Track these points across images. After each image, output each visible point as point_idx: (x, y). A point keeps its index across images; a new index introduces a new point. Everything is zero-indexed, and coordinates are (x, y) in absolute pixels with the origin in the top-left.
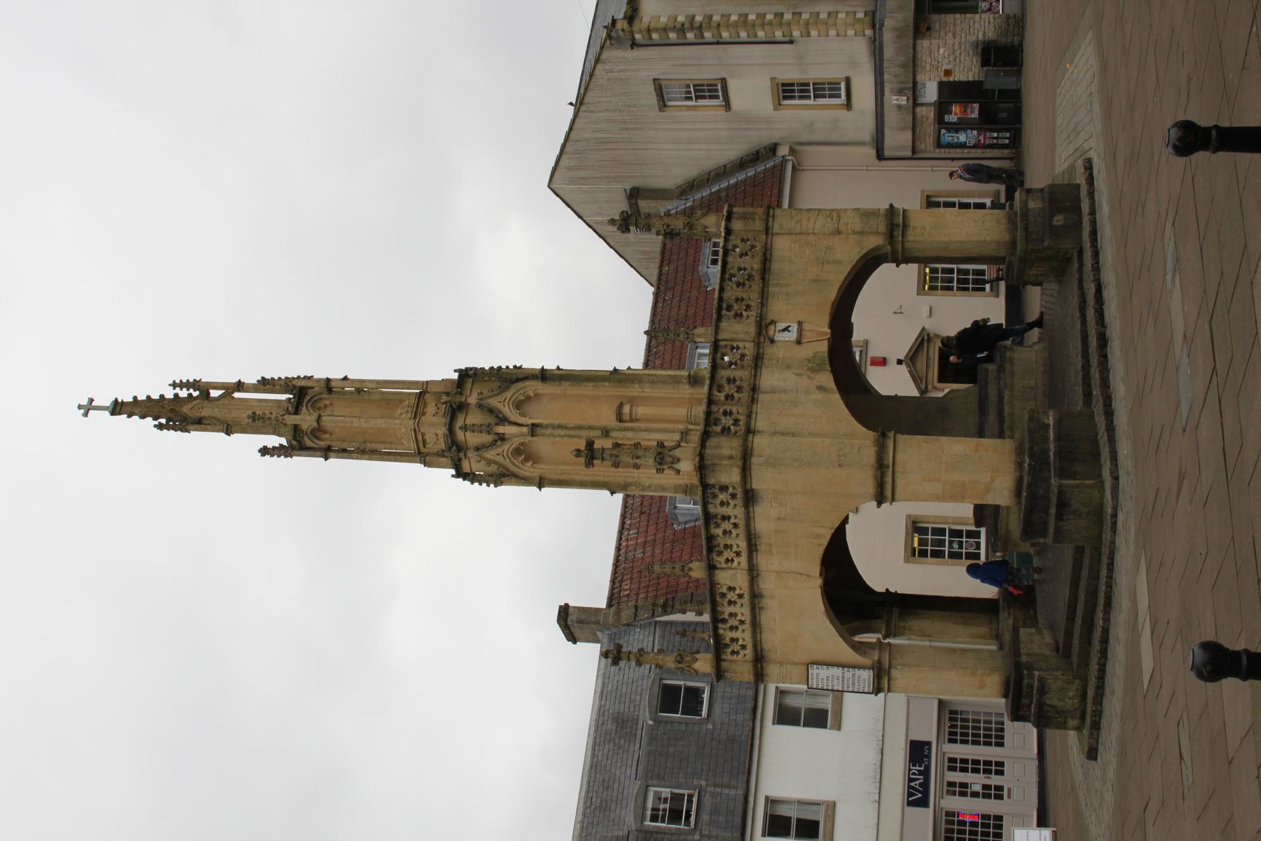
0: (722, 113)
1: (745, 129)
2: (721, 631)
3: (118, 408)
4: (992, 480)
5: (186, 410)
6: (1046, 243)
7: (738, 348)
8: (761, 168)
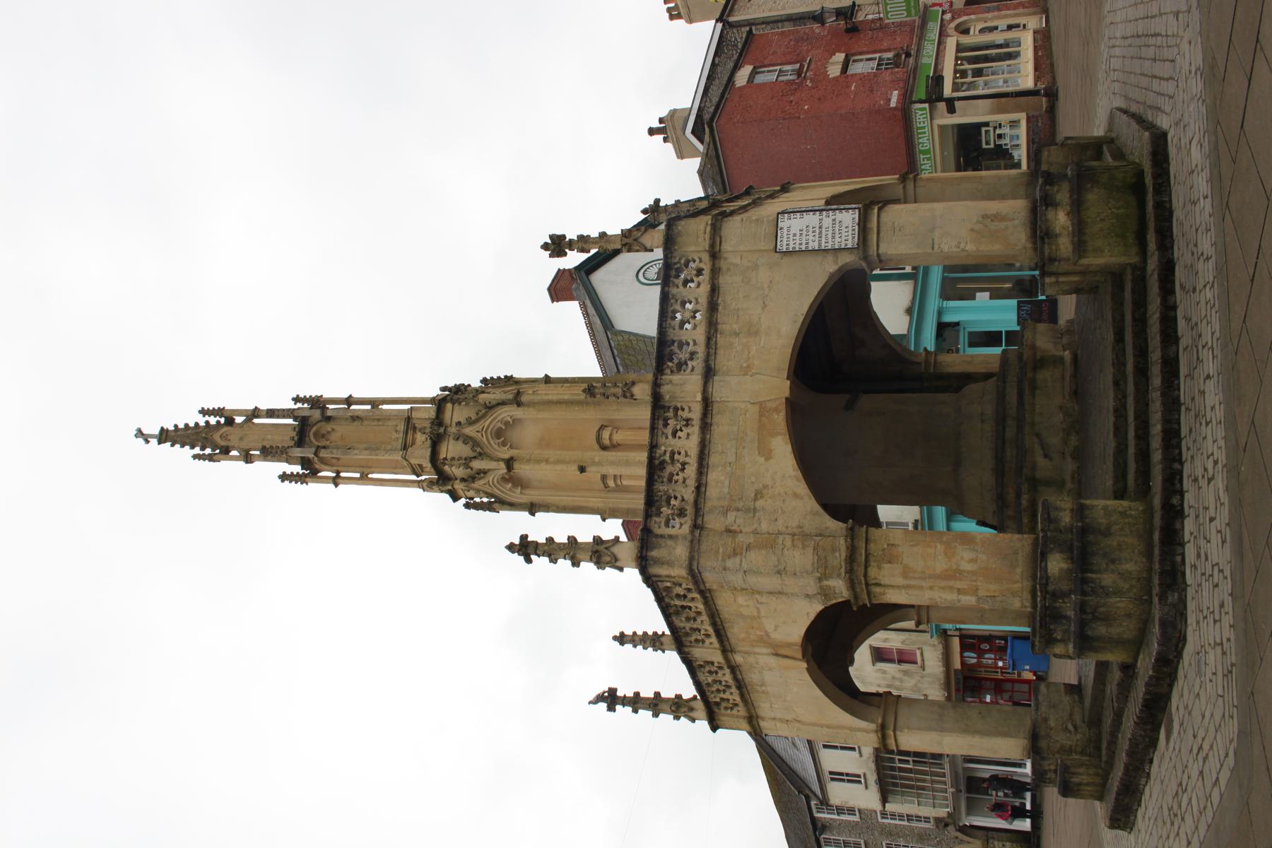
3: (165, 436)
5: (216, 436)
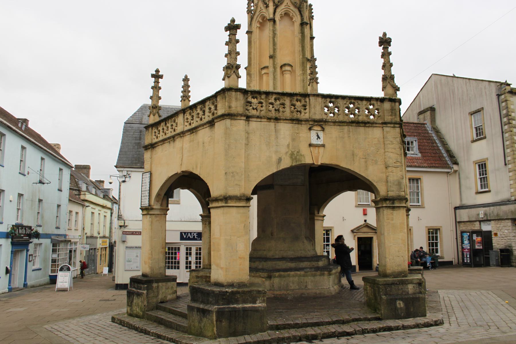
0: (470, 139)
1: (464, 150)
2: (162, 124)
4: (222, 268)
6: (384, 297)
7: (305, 109)
8: (447, 159)
